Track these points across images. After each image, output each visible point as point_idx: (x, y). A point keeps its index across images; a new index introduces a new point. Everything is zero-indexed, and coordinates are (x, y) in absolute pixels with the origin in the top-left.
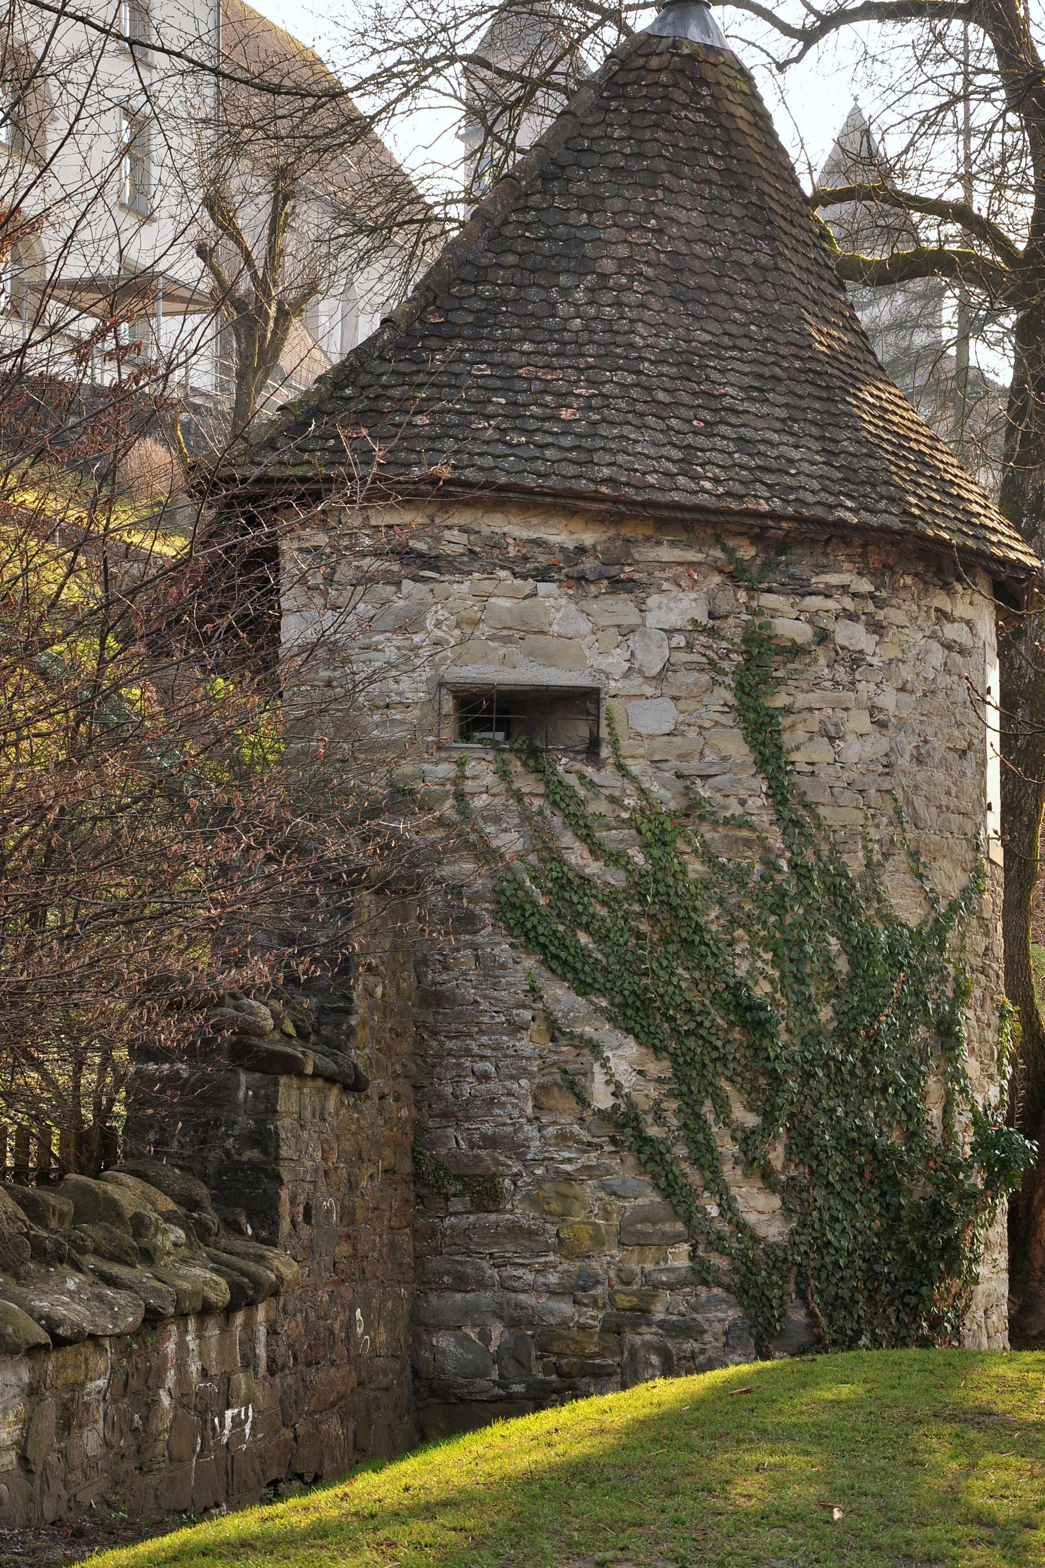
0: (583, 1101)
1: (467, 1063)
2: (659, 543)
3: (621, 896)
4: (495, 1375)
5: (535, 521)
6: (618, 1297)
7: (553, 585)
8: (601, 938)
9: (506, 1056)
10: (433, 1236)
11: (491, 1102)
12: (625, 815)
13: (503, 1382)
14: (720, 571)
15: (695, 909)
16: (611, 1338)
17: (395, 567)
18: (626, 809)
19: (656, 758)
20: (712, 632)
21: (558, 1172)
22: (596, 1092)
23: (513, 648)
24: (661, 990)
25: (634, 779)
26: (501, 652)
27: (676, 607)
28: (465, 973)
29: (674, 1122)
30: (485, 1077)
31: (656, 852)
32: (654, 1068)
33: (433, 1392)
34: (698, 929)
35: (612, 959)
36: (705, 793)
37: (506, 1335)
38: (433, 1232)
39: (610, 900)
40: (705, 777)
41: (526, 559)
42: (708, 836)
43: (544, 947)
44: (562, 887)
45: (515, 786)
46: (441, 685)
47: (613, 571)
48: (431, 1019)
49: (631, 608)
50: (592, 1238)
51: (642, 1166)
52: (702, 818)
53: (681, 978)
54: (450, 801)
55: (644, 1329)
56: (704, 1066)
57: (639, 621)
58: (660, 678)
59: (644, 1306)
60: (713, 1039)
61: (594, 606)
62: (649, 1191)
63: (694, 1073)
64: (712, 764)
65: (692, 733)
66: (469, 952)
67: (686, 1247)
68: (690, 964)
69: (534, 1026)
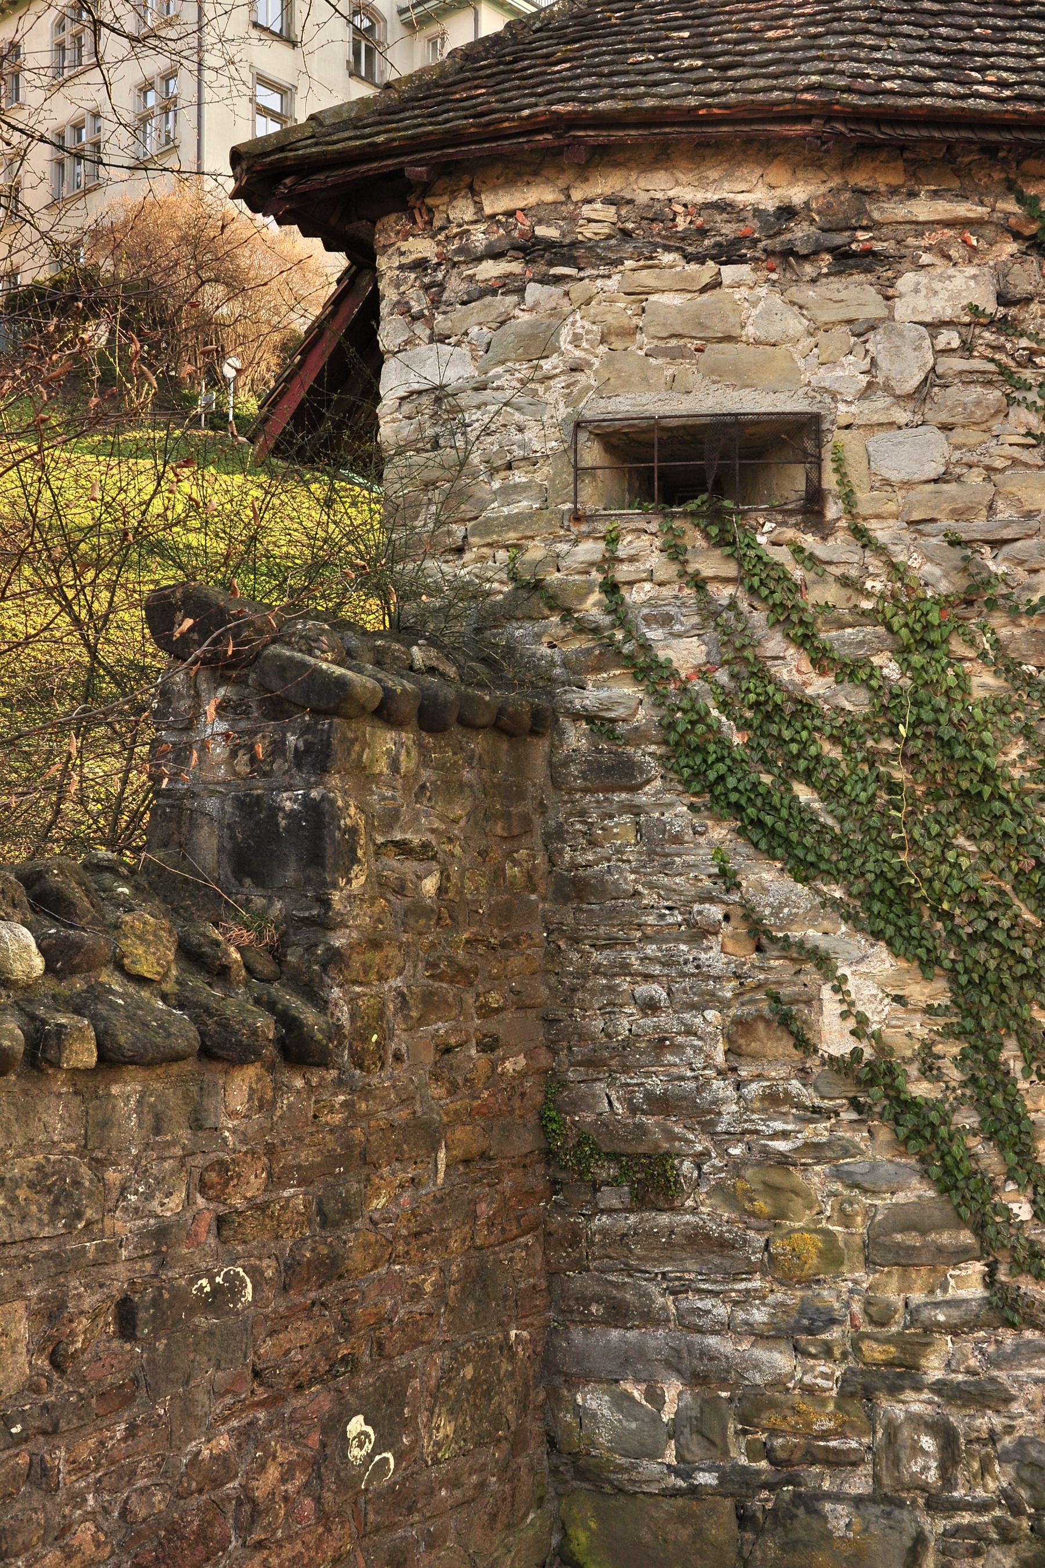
0: (804, 1044)
1: (624, 984)
2: (912, 195)
3: (861, 729)
4: (670, 1456)
5: (713, 174)
6: (864, 1346)
7: (745, 268)
8: (832, 793)
9: (683, 975)
10: (574, 1243)
11: (661, 1044)
12: (867, 605)
13: (684, 1469)
14: (1017, 236)
15: (983, 746)
16: (857, 1408)
17: (516, 267)
18: (869, 595)
19: (916, 516)
20: (1003, 325)
21: (765, 1151)
22: (825, 1030)
23: (687, 364)
24: (927, 872)
25: (881, 550)
26: (669, 372)
27: (945, 288)
28: (619, 851)
29: (955, 1075)
30: (650, 1006)
31: (917, 659)
32: (919, 992)
33: (581, 1474)
34: (988, 775)
35: (849, 825)
36: (998, 567)
37: (688, 1397)
38: (574, 1237)
39: (845, 733)
40: (996, 544)
41: (702, 232)
42: (1004, 633)
43: (739, 808)
44: (768, 717)
45: (691, 569)
46: (578, 425)
47: (839, 239)
48: (570, 919)
49: (871, 293)
50: (821, 1253)
51: (902, 1144)
52: (992, 604)
53: (962, 852)
54: (596, 596)
55: (909, 1395)
56: (1003, 988)
57: (883, 313)
58: (920, 395)
59: (909, 1360)
60: (1016, 946)
61: (810, 294)
62: (915, 1181)
63: (986, 1000)
64: (1007, 524)
65: (975, 478)
66: (627, 818)
67: (978, 1267)
68: (977, 830)
69: (727, 929)
